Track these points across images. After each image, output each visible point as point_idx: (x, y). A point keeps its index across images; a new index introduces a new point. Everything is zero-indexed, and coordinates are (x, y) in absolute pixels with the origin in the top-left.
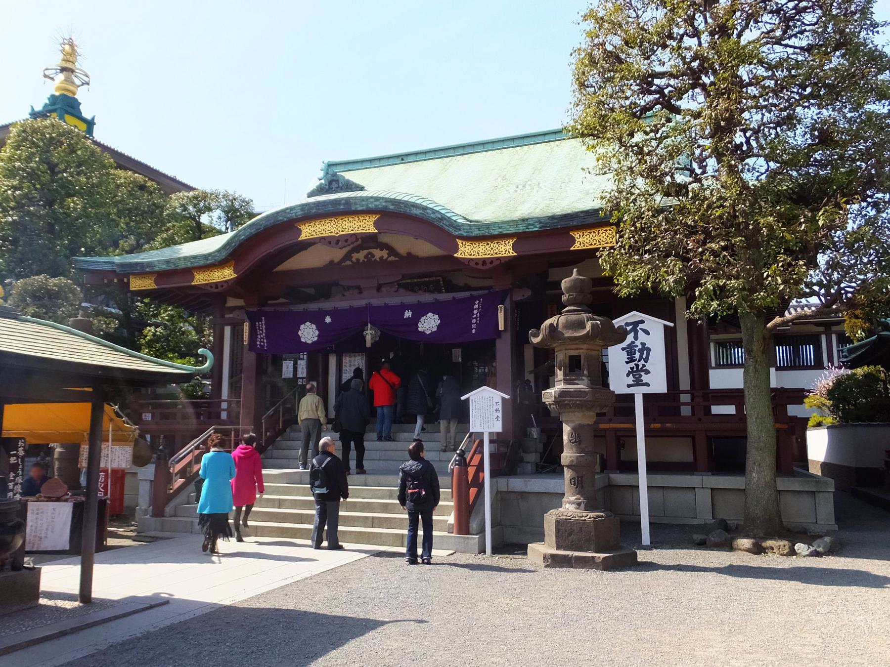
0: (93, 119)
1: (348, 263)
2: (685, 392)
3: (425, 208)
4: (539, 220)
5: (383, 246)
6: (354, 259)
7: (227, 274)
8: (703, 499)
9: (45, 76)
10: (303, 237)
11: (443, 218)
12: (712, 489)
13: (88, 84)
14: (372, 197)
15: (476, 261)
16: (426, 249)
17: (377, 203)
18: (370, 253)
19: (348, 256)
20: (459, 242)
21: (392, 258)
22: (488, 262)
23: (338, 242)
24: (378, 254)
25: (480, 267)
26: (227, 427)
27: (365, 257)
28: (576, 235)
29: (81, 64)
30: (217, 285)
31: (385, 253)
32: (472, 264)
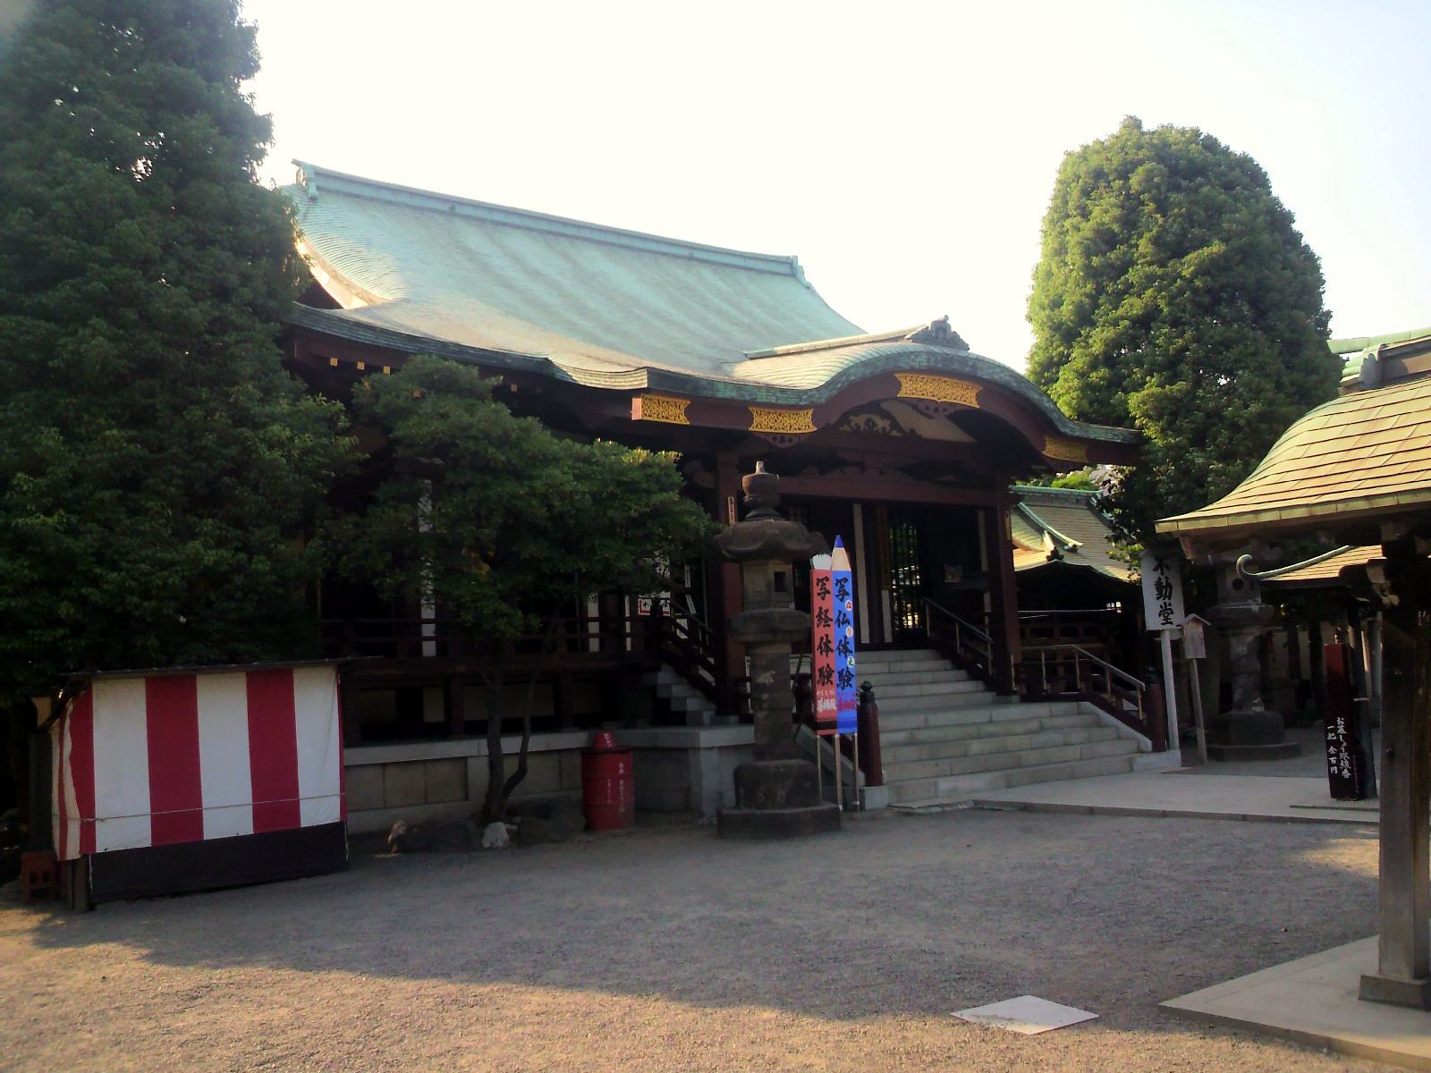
1: (846, 428)
2: (594, 620)
6: (853, 424)
17: (1002, 375)
32: (770, 439)
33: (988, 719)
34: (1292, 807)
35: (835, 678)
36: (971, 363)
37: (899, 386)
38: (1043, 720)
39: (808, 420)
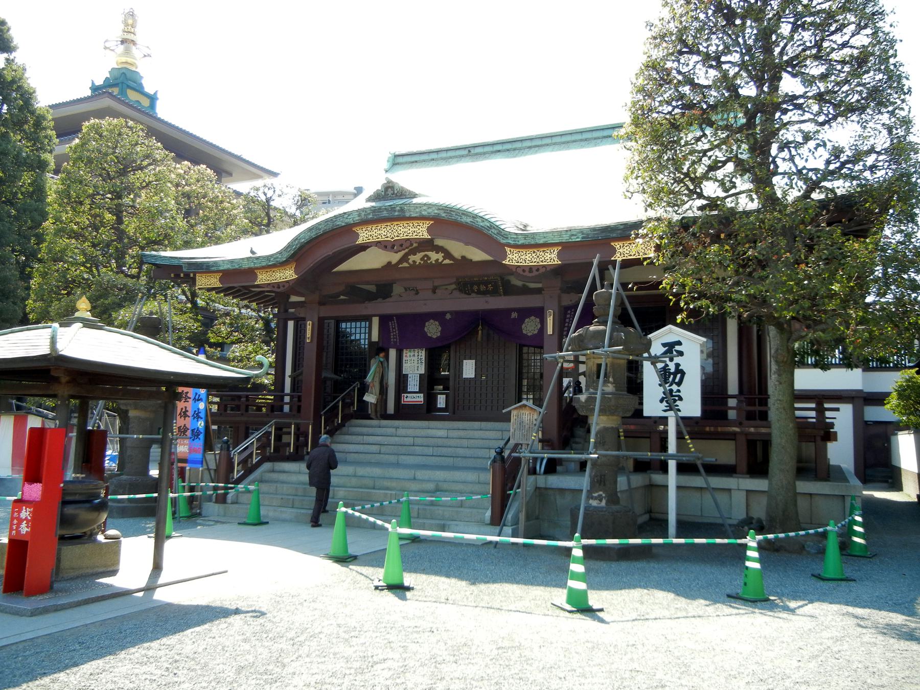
0: (156, 93)
1: (405, 265)
2: (733, 397)
3: (475, 216)
4: (581, 231)
5: (438, 249)
6: (410, 261)
7: (288, 274)
8: (739, 499)
9: (106, 48)
10: (360, 241)
11: (492, 226)
12: (748, 491)
13: (149, 56)
14: (425, 204)
15: (523, 268)
16: (477, 255)
17: (430, 210)
18: (426, 256)
19: (404, 259)
20: (508, 249)
21: (447, 261)
22: (534, 270)
23: (393, 247)
24: (434, 256)
25: (527, 274)
26: (682, 541)
27: (421, 259)
28: (617, 245)
29: (141, 35)
30: (278, 285)
31: (440, 256)
32: (520, 271)
33: (412, 477)
34: (226, 572)
35: (189, 433)
36: (398, 208)
37: (357, 235)
38: (440, 484)
39: (554, 255)
